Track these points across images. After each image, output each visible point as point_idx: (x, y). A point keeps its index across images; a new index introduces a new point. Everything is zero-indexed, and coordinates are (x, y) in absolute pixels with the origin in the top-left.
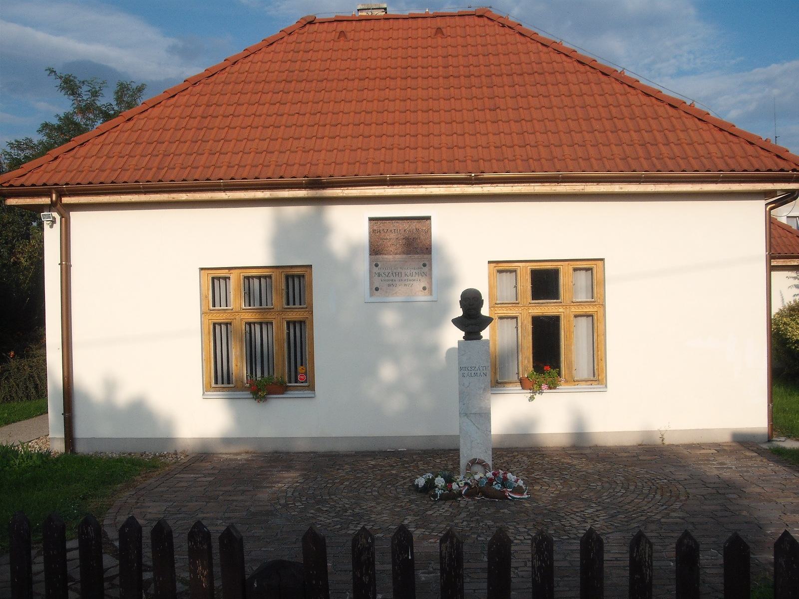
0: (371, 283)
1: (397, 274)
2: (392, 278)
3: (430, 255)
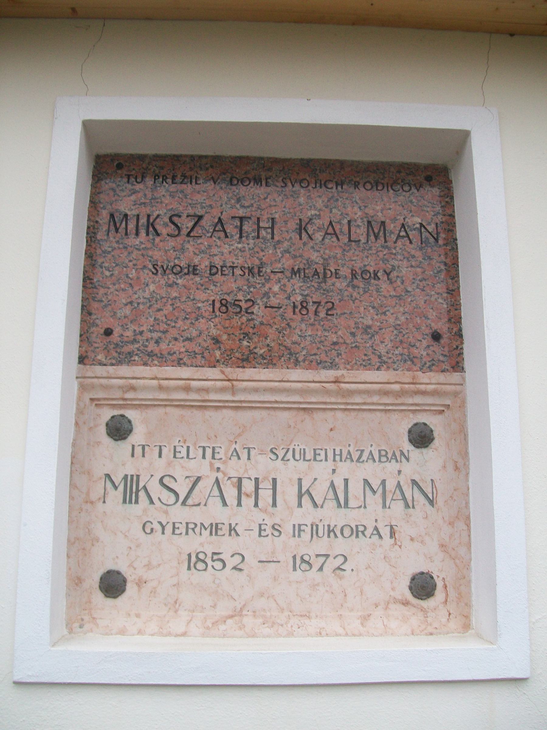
0: (78, 539)
1: (248, 486)
2: (215, 512)
3: (455, 377)
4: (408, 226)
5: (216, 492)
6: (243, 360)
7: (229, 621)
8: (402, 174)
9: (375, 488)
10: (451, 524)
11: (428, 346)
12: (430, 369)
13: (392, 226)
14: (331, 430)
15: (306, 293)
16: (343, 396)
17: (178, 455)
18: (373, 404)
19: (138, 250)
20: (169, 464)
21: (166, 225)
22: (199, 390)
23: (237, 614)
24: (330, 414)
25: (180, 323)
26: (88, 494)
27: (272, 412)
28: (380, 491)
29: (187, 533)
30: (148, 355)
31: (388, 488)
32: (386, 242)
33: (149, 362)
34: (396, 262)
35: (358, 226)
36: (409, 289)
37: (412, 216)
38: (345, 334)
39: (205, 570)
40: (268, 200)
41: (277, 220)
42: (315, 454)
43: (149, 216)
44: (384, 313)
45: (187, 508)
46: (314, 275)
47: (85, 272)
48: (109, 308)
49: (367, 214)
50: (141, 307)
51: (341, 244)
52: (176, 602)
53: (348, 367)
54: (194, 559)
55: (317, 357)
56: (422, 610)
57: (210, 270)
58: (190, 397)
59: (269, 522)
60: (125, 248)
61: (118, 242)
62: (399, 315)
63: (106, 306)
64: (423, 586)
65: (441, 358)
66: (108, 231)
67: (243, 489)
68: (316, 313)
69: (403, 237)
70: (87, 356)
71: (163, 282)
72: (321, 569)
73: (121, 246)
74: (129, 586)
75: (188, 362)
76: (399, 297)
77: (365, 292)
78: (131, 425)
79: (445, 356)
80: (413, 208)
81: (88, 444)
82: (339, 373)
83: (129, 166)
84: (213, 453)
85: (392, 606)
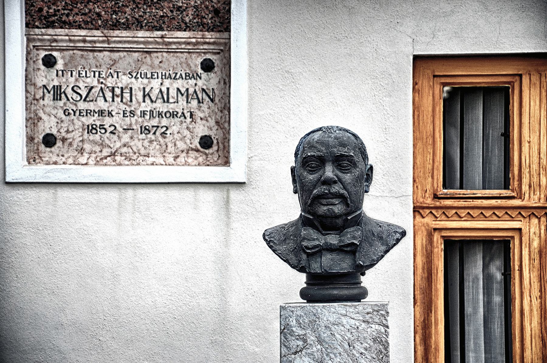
0: (33, 120)
1: (118, 91)
2: (101, 104)
5: (101, 94)
6: (113, 26)
7: (109, 158)
10: (221, 111)
12: (212, 31)
14: (160, 62)
16: (166, 45)
18: (182, 49)
20: (77, 80)
22: (90, 42)
25: (79, 5)
26: (34, 95)
27: (129, 53)
28: (185, 94)
29: (87, 115)
33: (64, 27)
39: (96, 133)
45: (86, 103)
53: (169, 29)
54: (90, 128)
56: (206, 154)
59: (128, 109)
64: (206, 142)
65: (218, 24)
72: (154, 133)
74: (58, 141)
75: (85, 27)
81: (34, 70)
82: (164, 33)
85: (190, 152)
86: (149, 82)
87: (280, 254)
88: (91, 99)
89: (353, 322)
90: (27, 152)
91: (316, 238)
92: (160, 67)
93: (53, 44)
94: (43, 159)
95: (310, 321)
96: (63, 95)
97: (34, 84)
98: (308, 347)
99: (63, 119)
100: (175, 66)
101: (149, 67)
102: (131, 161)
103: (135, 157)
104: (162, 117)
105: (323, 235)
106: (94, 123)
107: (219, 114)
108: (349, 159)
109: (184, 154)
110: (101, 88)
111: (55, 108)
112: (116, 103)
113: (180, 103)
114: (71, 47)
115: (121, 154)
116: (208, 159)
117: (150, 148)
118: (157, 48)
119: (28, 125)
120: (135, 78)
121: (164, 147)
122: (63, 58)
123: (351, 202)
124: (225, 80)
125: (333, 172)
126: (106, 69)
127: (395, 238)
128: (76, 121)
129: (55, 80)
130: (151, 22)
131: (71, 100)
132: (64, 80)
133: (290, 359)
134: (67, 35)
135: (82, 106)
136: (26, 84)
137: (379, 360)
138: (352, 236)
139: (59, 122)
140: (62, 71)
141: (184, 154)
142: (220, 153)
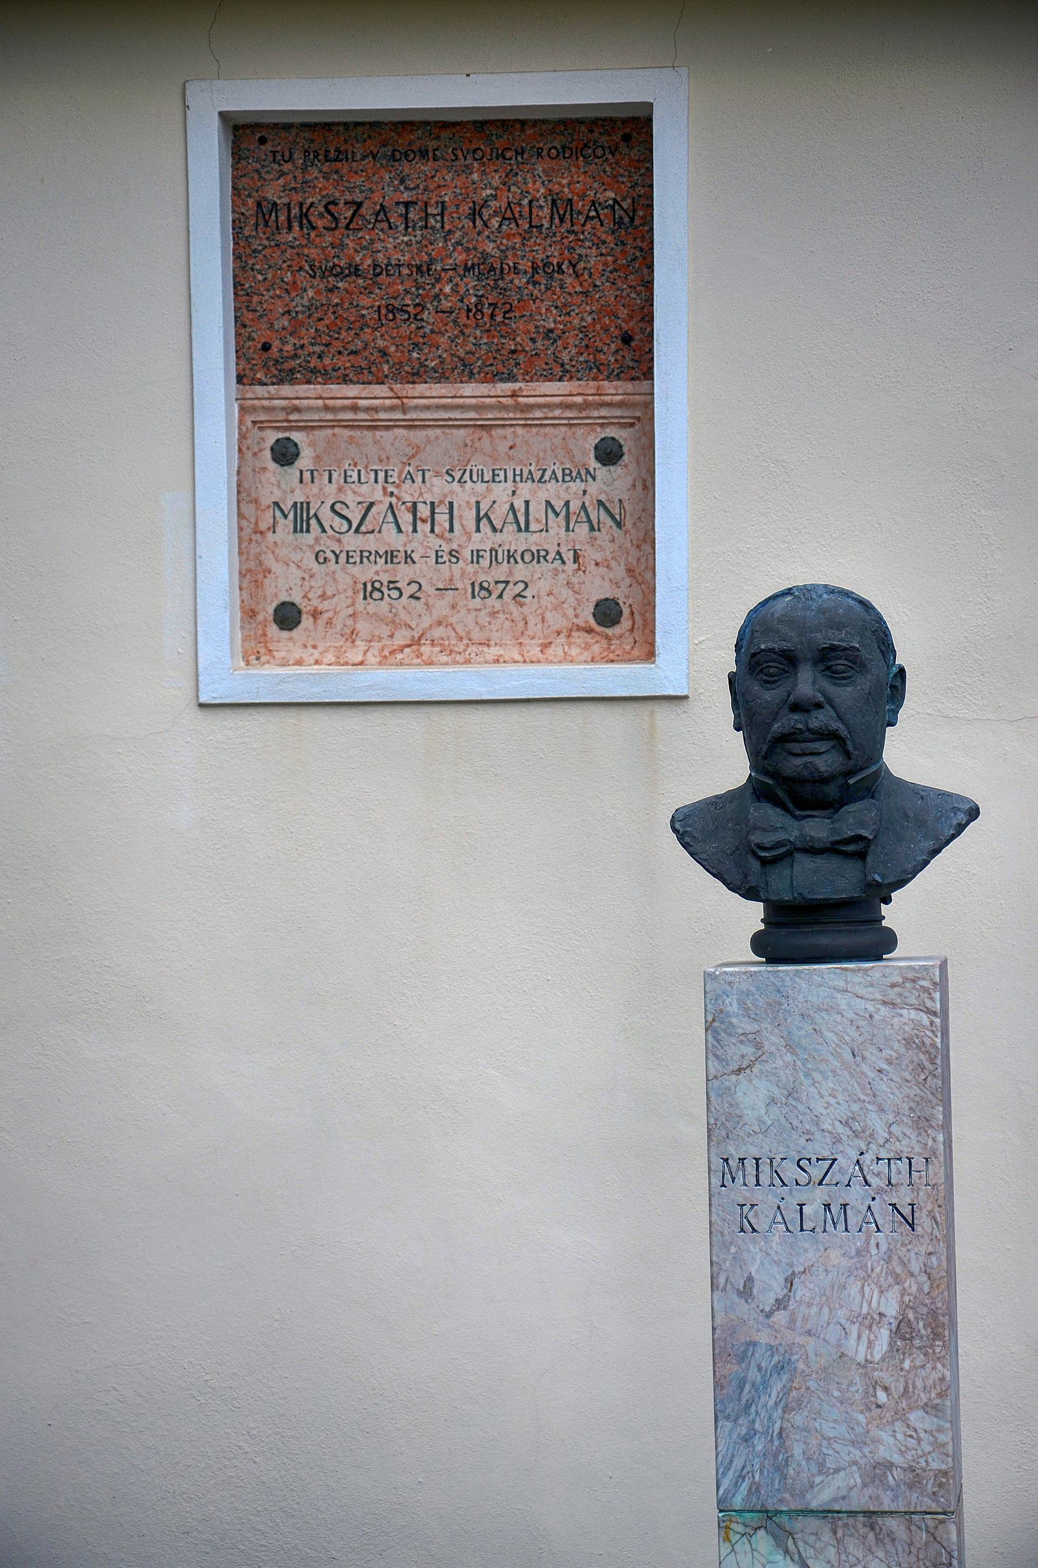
0: (251, 575)
1: (424, 511)
2: (390, 538)
4: (600, 204)
5: (390, 518)
6: (413, 374)
7: (407, 650)
8: (595, 134)
9: (558, 510)
10: (638, 547)
11: (617, 351)
12: (618, 377)
13: (581, 204)
14: (511, 448)
15: (480, 293)
16: (522, 411)
17: (349, 480)
18: (554, 418)
19: (292, 247)
20: (340, 489)
21: (321, 216)
22: (367, 409)
23: (416, 643)
24: (509, 431)
25: (344, 334)
26: (256, 524)
27: (447, 431)
28: (564, 513)
29: (361, 562)
30: (311, 371)
31: (572, 510)
32: (572, 225)
33: (313, 380)
34: (584, 251)
35: (541, 207)
36: (598, 283)
37: (605, 190)
38: (523, 340)
39: (382, 599)
40: (436, 179)
41: (447, 204)
42: (494, 475)
43: (301, 205)
44: (568, 314)
45: (361, 536)
46: (490, 271)
47: (235, 276)
48: (265, 319)
49: (550, 190)
50: (300, 316)
51: (520, 231)
52: (352, 633)
53: (527, 378)
54: (369, 588)
55: (493, 368)
56: (608, 638)
57: (374, 270)
58: (358, 417)
59: (446, 548)
60: (277, 245)
61: (268, 239)
62: (585, 315)
63: (261, 316)
64: (607, 613)
65: (631, 364)
66: (257, 225)
67: (419, 514)
68: (492, 316)
69: (592, 218)
70: (245, 375)
71: (322, 286)
72: (500, 596)
73: (273, 243)
74: (304, 617)
75: (355, 379)
76: (586, 294)
77: (547, 289)
78: (298, 449)
79: (636, 361)
80: (606, 180)
81: (254, 470)
82: (517, 386)
83: (274, 140)
84: (386, 476)
85: (575, 634)
86: (488, 490)
87: (705, 860)
88: (370, 528)
89: (860, 1004)
90: (244, 641)
91: (779, 825)
92: (510, 458)
93: (292, 417)
94: (275, 654)
95: (769, 1004)
96: (313, 522)
97: (256, 501)
98: (764, 1057)
99: (314, 571)
100: (541, 454)
101: (488, 459)
102: (454, 655)
103: (461, 647)
104: (516, 562)
105: (795, 817)
106: (376, 578)
107: (634, 552)
108: (850, 655)
109: (562, 639)
110: (391, 504)
111: (298, 548)
112: (419, 535)
113: (552, 532)
114: (329, 421)
115: (433, 641)
116: (612, 647)
117: (492, 626)
118: (504, 419)
119: (245, 585)
120: (459, 481)
121: (521, 624)
122: (312, 444)
123: (855, 748)
124: (645, 480)
125: (814, 683)
126: (400, 465)
127: (955, 822)
128: (339, 575)
129: (298, 491)
130: (491, 365)
131: (330, 532)
132: (315, 490)
133: (727, 1083)
134: (320, 398)
135: (353, 542)
136: (239, 501)
137: (918, 1084)
138: (856, 819)
139: (307, 577)
140: (312, 472)
141: (562, 639)
142: (637, 634)
